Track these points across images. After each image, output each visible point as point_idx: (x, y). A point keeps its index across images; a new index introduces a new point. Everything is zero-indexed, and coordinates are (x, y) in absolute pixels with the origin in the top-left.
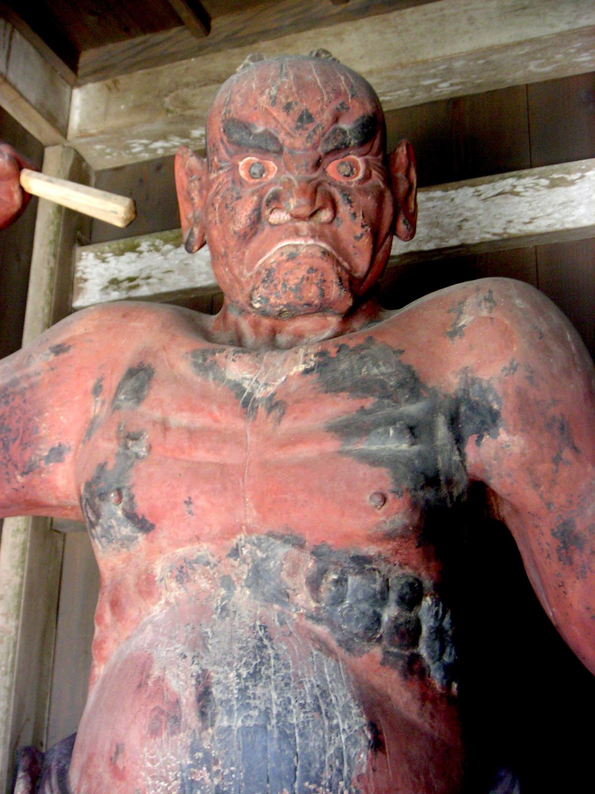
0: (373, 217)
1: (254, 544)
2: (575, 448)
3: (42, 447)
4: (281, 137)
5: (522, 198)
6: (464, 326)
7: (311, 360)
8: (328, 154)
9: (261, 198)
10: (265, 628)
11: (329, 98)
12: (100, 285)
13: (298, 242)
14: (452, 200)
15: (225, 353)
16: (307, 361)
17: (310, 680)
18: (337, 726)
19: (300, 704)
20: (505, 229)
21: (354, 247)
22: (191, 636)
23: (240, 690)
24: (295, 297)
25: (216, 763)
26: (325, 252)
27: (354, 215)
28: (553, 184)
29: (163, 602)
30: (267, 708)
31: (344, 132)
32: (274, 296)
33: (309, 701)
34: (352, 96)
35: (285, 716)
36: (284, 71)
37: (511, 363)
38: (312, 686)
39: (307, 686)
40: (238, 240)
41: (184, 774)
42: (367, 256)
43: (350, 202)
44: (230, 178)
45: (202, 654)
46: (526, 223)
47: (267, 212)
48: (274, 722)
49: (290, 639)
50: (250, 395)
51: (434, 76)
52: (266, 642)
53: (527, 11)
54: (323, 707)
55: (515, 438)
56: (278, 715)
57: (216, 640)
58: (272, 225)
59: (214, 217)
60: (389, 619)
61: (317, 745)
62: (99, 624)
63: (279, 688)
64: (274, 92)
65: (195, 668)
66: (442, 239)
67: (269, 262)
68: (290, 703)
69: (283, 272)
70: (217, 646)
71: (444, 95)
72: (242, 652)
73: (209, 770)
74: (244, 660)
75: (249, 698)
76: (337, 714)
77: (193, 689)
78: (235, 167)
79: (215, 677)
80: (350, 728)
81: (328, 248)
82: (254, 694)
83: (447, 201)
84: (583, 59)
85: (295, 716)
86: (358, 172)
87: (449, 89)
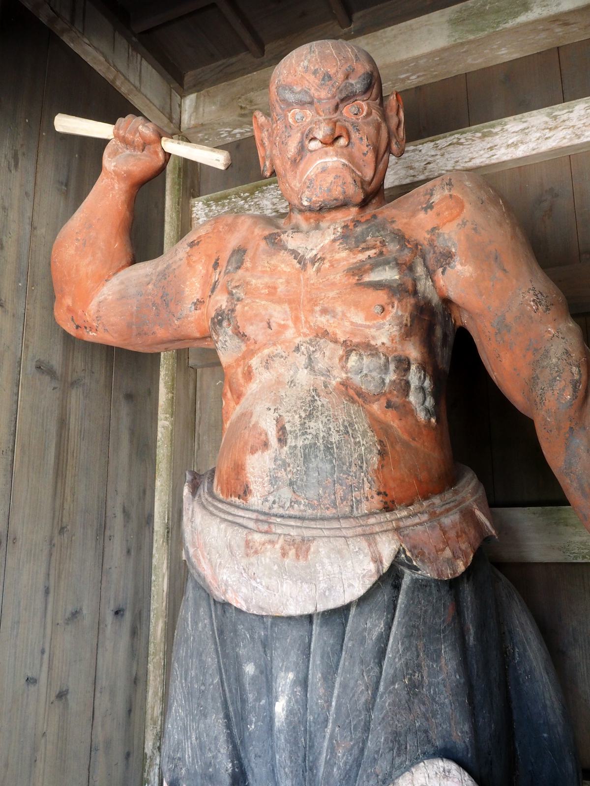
0: (374, 141)
1: (308, 343)
2: (505, 270)
3: (187, 302)
4: (313, 91)
5: (465, 146)
6: (433, 202)
7: (338, 232)
8: (342, 100)
9: (302, 134)
10: (316, 390)
11: (341, 64)
12: (395, 513)
13: (327, 160)
14: (420, 151)
15: (287, 234)
16: (336, 232)
17: (342, 417)
18: (359, 442)
19: (337, 431)
20: (454, 167)
21: (363, 161)
22: (259, 386)
23: (301, 424)
24: (327, 195)
25: (289, 466)
26: (344, 165)
27: (361, 138)
28: (484, 136)
29: (258, 381)
30: (317, 434)
31: (352, 85)
32: (314, 196)
33: (342, 428)
34: (356, 60)
35: (328, 438)
36: (313, 50)
37: (463, 221)
38: (344, 420)
39: (341, 421)
40: (291, 163)
41: (272, 474)
42: (372, 165)
43: (358, 130)
44: (284, 125)
45: (280, 407)
46: (466, 162)
47: (307, 143)
48: (321, 441)
49: (331, 395)
50: (303, 256)
51: (407, 71)
52: (316, 398)
53: (466, 22)
54: (350, 432)
55: (466, 267)
56: (324, 437)
57: (288, 399)
58: (311, 151)
59: (276, 152)
60: (390, 381)
61: (346, 453)
62: (225, 398)
63: (324, 422)
64: (306, 63)
65: (276, 415)
66: (414, 176)
67: (310, 175)
68: (330, 430)
69: (319, 180)
70: (289, 402)
71: (414, 84)
72: (302, 404)
73: (285, 470)
74: (304, 408)
75: (307, 428)
76: (359, 435)
77: (275, 427)
78: (286, 116)
79: (286, 419)
80: (367, 443)
81: (347, 163)
82: (309, 426)
83: (417, 152)
84: (503, 52)
85: (333, 437)
86: (363, 111)
87: (417, 80)
